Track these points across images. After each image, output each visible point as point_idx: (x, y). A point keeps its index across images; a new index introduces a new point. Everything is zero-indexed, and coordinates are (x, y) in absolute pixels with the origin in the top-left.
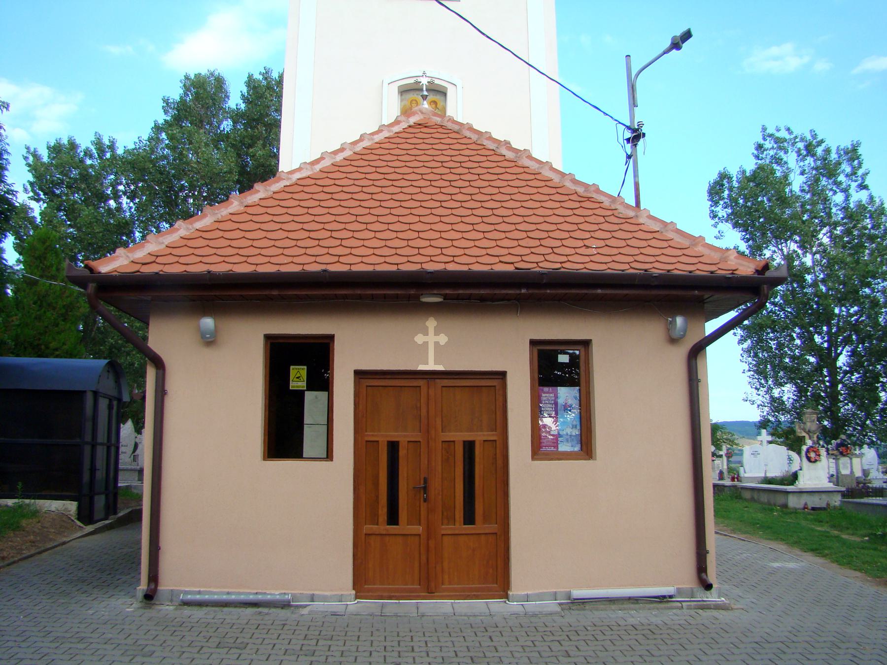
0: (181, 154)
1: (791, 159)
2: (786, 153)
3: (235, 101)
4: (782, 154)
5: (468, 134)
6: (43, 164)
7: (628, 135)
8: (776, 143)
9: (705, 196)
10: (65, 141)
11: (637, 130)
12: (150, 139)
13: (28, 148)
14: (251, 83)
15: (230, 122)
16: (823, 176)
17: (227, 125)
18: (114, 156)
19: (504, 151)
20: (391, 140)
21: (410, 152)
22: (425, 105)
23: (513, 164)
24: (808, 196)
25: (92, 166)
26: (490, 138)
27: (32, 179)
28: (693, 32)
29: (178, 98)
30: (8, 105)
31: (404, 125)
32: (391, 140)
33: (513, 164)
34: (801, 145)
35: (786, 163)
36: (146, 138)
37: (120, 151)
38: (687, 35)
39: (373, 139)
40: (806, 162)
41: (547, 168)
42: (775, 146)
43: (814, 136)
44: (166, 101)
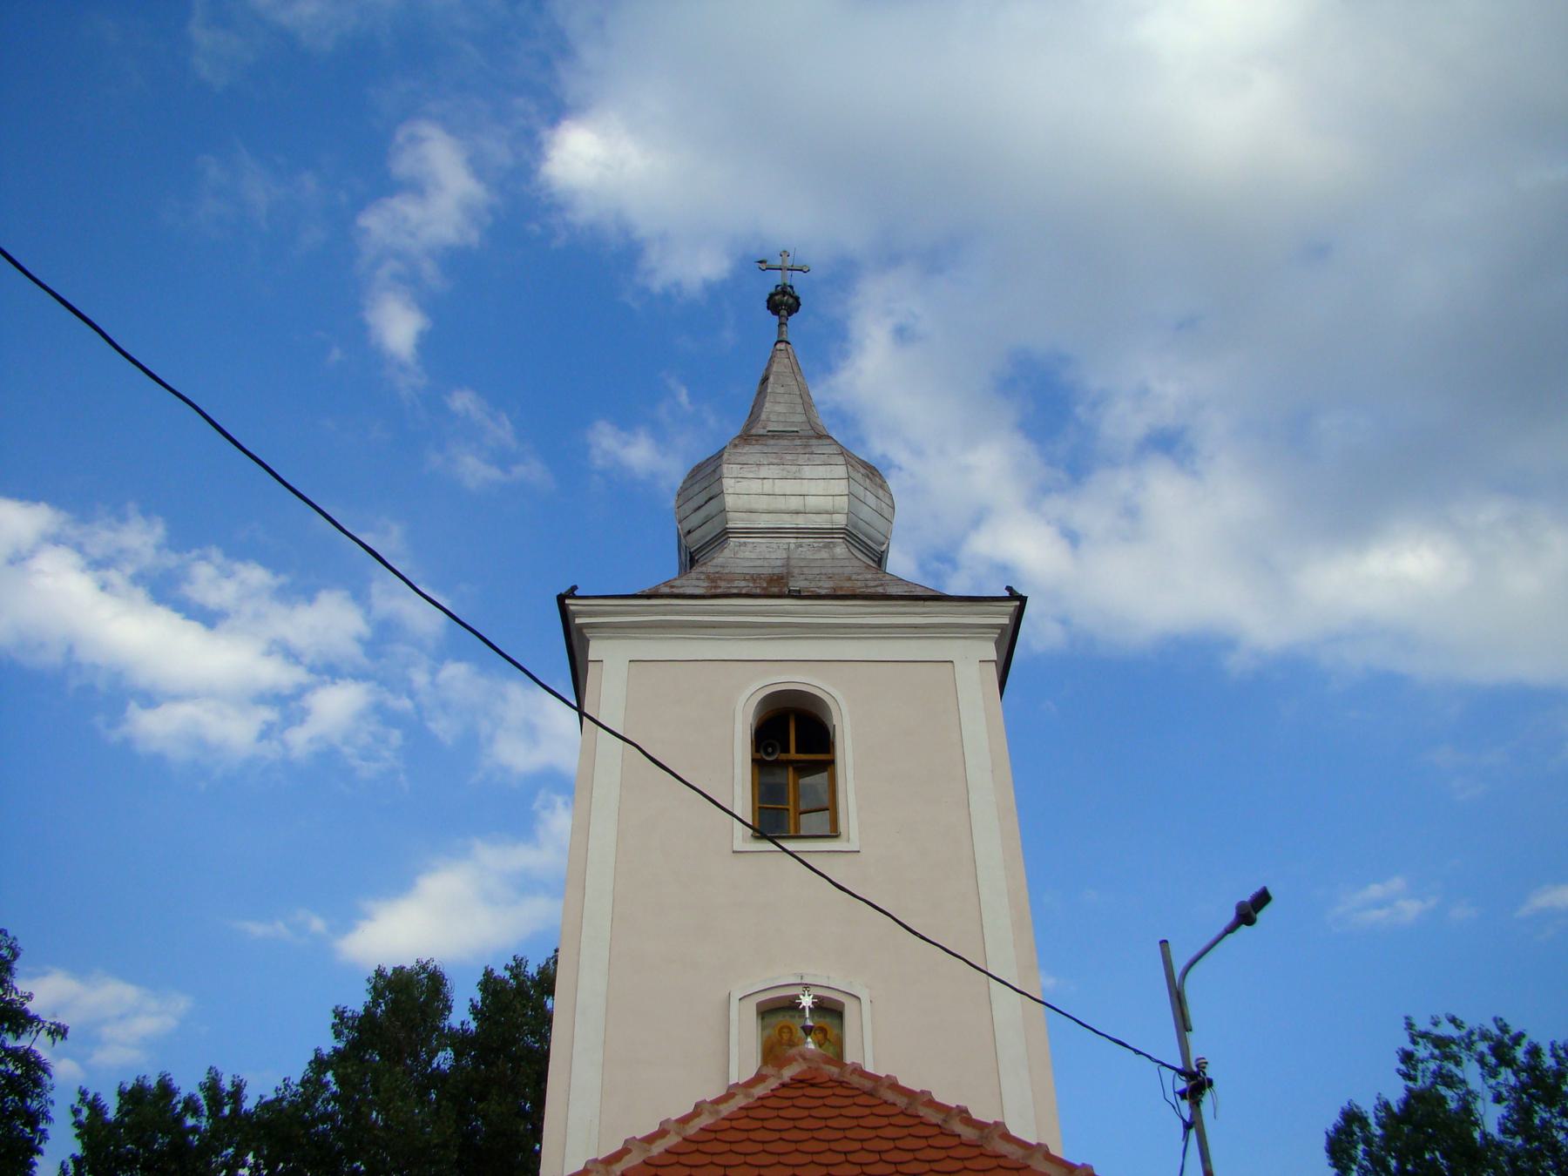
0: (357, 1110)
1: (1471, 1073)
2: (1458, 1063)
3: (460, 1016)
4: (1451, 1066)
5: (889, 1096)
6: (106, 1123)
7: (1182, 1084)
8: (1436, 1046)
9: (1323, 1158)
10: (153, 1082)
11: (1197, 1074)
12: (304, 1083)
13: (84, 1093)
14: (489, 983)
15: (450, 1053)
16: (1538, 1101)
17: (444, 1059)
18: (236, 1111)
19: (958, 1127)
20: (751, 1113)
21: (785, 1135)
22: (811, 1044)
23: (975, 1152)
24: (1519, 1141)
25: (195, 1129)
26: (932, 1103)
27: (79, 1151)
28: (1271, 891)
29: (360, 1010)
30: (66, 1030)
31: (773, 1083)
32: (751, 1113)
33: (975, 1152)
34: (1482, 1047)
35: (1463, 1082)
36: (297, 1080)
37: (249, 1104)
38: (1262, 898)
39: (717, 1112)
40: (1501, 1079)
41: (1039, 1156)
42: (1436, 1052)
43: (1504, 1029)
44: (339, 1014)
